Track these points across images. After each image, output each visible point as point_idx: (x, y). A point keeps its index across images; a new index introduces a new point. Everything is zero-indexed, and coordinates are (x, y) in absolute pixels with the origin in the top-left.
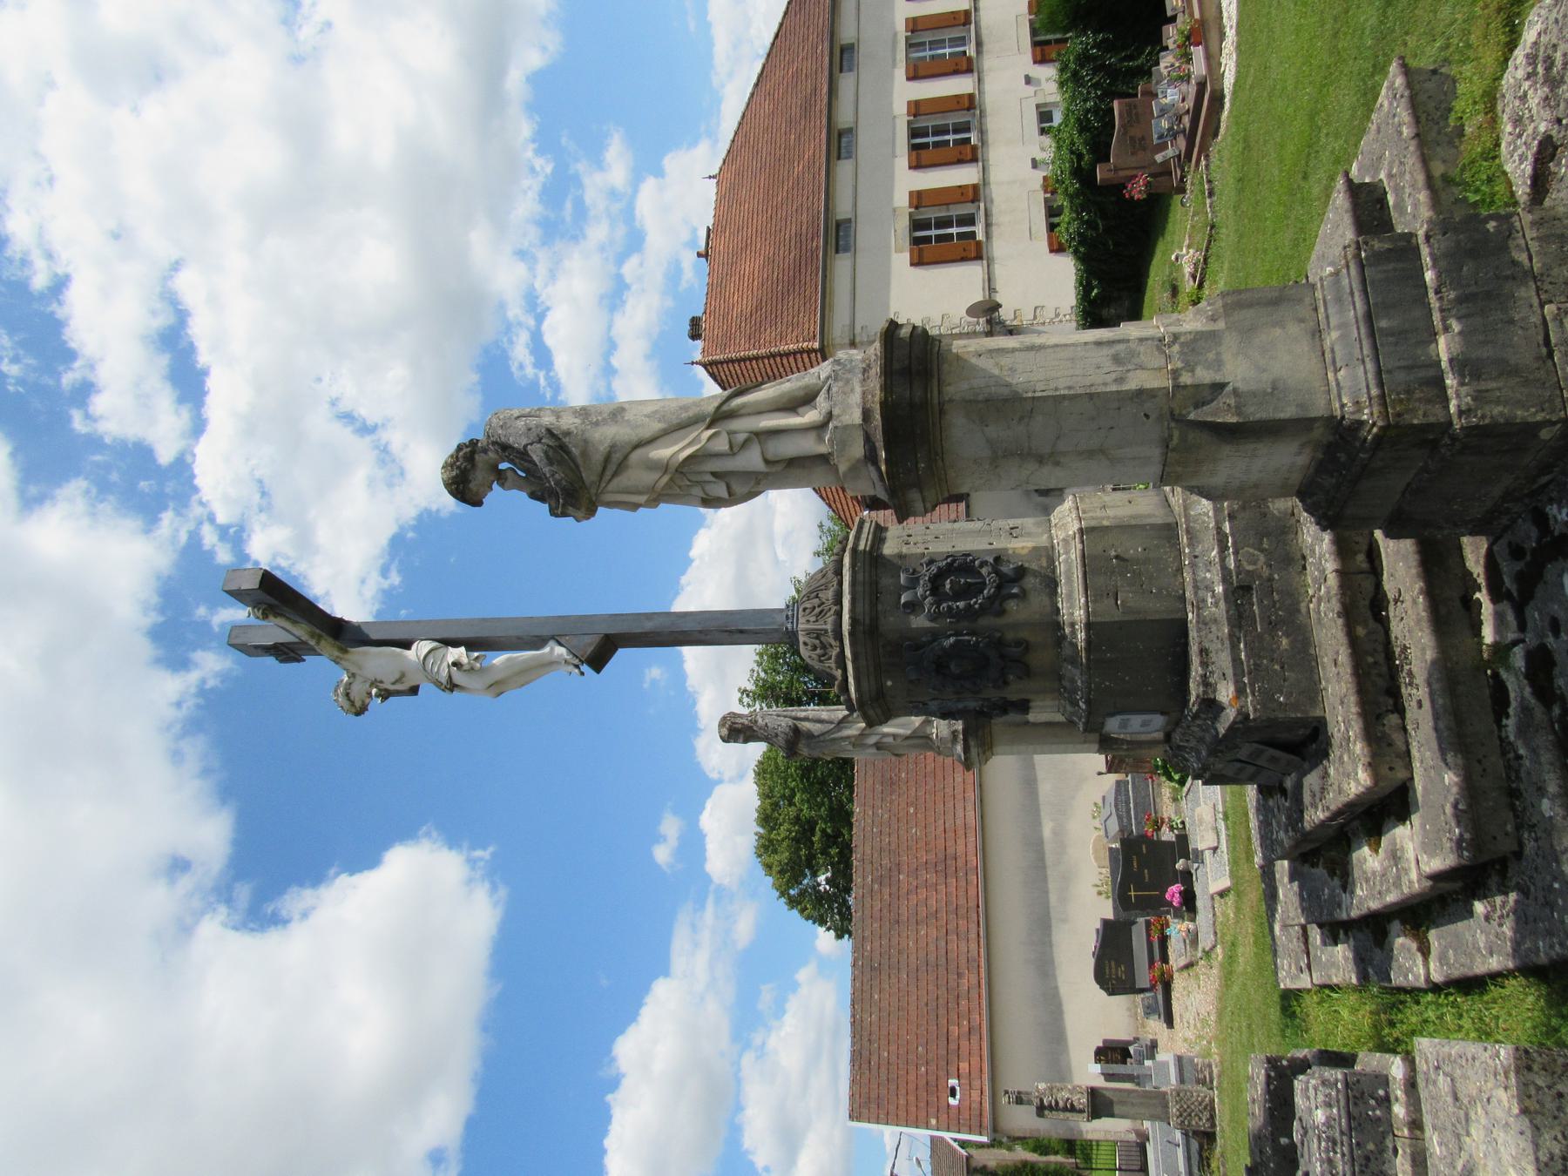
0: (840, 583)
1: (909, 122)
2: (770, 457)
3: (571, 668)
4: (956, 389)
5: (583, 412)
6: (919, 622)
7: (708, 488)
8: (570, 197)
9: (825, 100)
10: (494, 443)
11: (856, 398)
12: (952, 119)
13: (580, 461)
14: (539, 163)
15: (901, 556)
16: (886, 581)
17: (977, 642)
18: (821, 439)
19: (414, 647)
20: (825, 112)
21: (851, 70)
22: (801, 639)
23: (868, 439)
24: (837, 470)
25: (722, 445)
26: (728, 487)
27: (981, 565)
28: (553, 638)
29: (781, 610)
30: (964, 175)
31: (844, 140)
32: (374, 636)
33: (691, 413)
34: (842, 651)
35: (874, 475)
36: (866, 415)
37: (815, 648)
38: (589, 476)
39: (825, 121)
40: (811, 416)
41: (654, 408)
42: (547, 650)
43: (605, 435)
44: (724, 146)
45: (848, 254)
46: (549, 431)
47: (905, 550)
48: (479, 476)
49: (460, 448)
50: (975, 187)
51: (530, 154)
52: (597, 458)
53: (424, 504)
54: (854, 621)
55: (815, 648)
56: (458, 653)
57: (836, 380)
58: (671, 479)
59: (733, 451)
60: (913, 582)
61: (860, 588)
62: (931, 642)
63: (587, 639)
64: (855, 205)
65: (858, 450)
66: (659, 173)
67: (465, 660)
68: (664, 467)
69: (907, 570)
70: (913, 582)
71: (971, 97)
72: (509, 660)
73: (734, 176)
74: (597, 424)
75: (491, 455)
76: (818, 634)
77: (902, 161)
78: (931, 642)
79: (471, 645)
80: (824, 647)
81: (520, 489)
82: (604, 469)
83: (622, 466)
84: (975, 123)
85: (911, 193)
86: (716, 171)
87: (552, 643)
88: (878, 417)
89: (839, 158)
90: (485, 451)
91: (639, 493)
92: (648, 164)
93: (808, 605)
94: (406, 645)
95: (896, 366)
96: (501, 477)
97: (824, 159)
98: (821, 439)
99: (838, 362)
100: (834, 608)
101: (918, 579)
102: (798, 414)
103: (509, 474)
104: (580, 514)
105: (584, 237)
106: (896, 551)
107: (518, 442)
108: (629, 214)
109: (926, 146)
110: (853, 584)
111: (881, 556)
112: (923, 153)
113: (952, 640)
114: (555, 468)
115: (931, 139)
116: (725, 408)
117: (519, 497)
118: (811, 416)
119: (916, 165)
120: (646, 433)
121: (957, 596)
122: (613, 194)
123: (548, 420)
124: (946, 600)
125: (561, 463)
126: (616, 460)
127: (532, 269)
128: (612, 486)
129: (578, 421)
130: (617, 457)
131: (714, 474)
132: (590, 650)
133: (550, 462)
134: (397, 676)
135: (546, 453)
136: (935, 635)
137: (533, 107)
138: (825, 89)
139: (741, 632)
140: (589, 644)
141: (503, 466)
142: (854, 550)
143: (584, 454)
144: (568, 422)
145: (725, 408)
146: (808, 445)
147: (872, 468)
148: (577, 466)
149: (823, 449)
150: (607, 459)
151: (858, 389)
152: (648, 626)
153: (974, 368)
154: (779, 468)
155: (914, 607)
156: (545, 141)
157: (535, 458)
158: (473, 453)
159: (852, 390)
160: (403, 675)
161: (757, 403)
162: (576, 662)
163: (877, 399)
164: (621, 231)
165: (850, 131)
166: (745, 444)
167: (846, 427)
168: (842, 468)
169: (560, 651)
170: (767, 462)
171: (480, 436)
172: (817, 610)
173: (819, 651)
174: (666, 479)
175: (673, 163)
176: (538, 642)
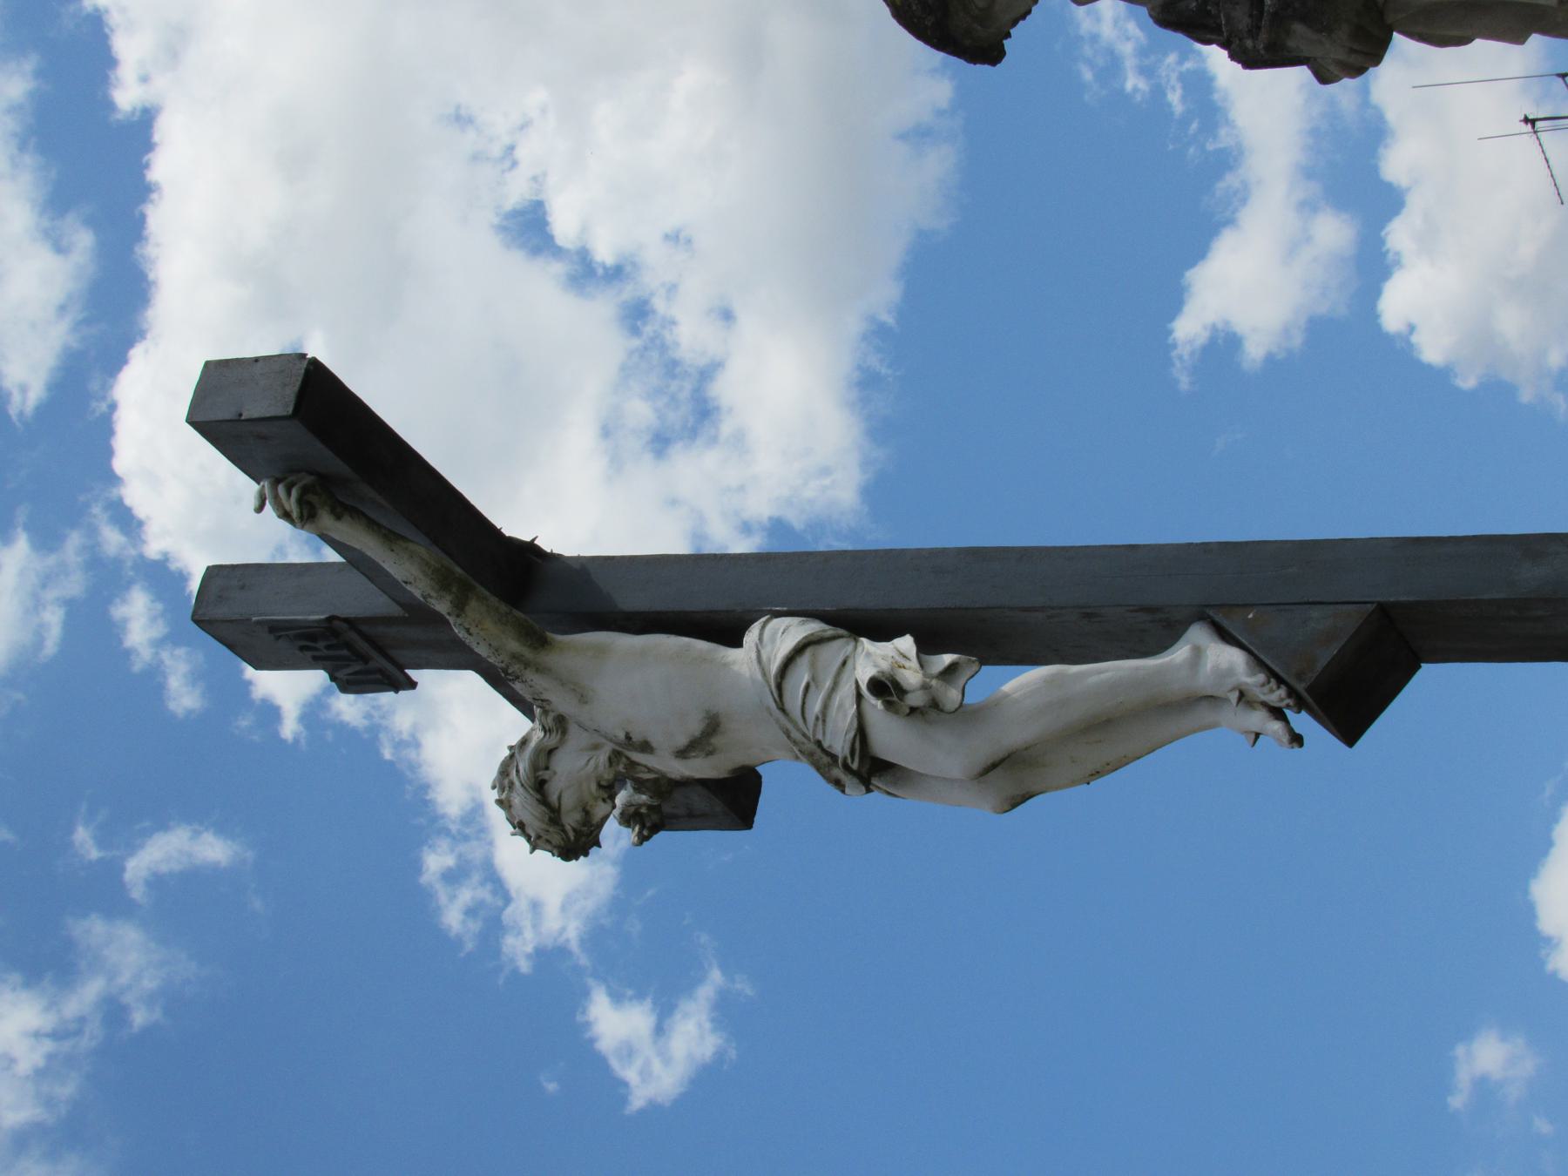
19: (751, 637)
42: (1179, 654)
67: (911, 676)
72: (1050, 681)
87: (1198, 634)
134: (695, 727)
140: (1324, 634)
160: (713, 725)
162: (1277, 696)
176: (1155, 632)
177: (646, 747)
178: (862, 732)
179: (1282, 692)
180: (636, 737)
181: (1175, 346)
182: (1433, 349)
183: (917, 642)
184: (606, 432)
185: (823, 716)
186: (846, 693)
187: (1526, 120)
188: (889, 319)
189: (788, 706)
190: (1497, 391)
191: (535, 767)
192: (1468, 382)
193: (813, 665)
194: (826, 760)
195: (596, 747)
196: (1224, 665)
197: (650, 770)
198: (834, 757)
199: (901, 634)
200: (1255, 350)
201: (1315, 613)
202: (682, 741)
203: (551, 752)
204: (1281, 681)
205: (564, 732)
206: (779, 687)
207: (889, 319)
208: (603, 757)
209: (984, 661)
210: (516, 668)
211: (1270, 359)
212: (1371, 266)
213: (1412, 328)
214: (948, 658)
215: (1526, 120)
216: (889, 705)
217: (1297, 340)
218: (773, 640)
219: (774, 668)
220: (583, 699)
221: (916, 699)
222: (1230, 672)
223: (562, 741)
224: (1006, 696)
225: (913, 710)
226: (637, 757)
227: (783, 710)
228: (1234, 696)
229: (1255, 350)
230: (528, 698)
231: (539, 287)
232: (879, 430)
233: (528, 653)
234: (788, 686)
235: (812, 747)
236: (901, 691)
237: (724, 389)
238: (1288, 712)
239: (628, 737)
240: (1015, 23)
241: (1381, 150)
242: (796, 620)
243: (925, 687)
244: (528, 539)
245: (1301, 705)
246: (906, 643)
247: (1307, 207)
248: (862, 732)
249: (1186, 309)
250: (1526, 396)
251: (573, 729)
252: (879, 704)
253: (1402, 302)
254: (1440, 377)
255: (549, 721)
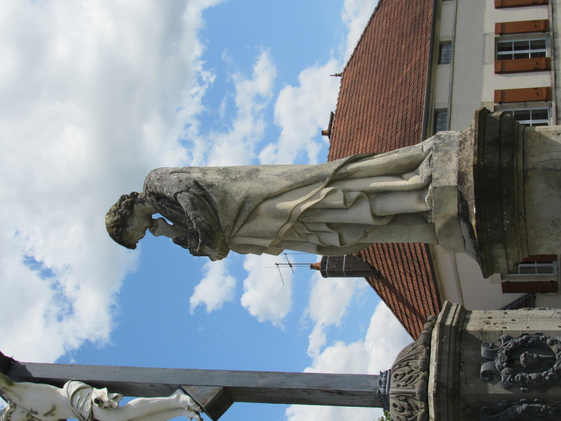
0: (429, 353)
1: (496, 39)
2: (378, 212)
3: (192, 414)
4: (538, 159)
5: (225, 171)
6: (496, 389)
7: (322, 236)
8: (225, 98)
9: (430, 20)
10: (152, 193)
11: (453, 166)
12: (530, 39)
13: (219, 208)
14: (206, 75)
15: (482, 332)
16: (468, 353)
17: (546, 410)
18: (421, 199)
19: (66, 386)
20: (430, 28)
21: (448, 63)
22: (392, 401)
23: (462, 199)
24: (434, 229)
25: (337, 200)
26: (340, 237)
27: (552, 343)
28: (180, 387)
29: (375, 377)
30: (539, 80)
31: (444, 50)
32: (35, 375)
33: (313, 174)
34: (427, 412)
35: (465, 232)
36: (461, 177)
37: (403, 410)
38: (225, 221)
39: (429, 35)
40: (414, 180)
41: (285, 170)
42: (174, 396)
43: (240, 189)
44: (347, 58)
45: (448, 65)
46: (196, 183)
47: (486, 328)
48: (136, 222)
49: (123, 198)
50: (548, 90)
51: (199, 68)
52: (233, 206)
53: (84, 336)
54: (439, 384)
55: (403, 410)
56: (102, 393)
57: (436, 151)
58: (293, 227)
59: (347, 206)
60: (492, 355)
61: (445, 357)
62: (506, 407)
63: (209, 390)
64: (451, 98)
65: (452, 208)
66: (296, 84)
67: (106, 398)
68: (287, 216)
69: (487, 345)
70: (492, 355)
71: (546, 22)
72: (141, 402)
73: (354, 77)
74: (235, 180)
75: (147, 205)
76: (406, 397)
77: (490, 68)
78: (506, 407)
79: (112, 388)
80: (411, 409)
81: (168, 235)
82: (238, 216)
83: (253, 214)
84: (548, 42)
85: (496, 92)
86: (342, 71)
87: (179, 391)
88: (471, 178)
89: (439, 63)
90: (143, 201)
91: (265, 237)
92: (287, 76)
93: (399, 372)
94: (60, 384)
95: (488, 138)
96: (153, 226)
97: (427, 63)
98: (421, 199)
99: (439, 137)
100: (422, 374)
101: (496, 352)
102: (403, 179)
103: (160, 223)
104: (215, 254)
105: (232, 128)
106: (478, 328)
107: (169, 191)
108: (269, 114)
109: (510, 56)
110: (440, 352)
111: (465, 332)
112: (507, 62)
113: (524, 406)
114: (198, 212)
115: (513, 52)
116: (342, 171)
117: (166, 242)
118: (414, 180)
119: (500, 71)
120: (276, 188)
121: (529, 369)
122: (258, 98)
123: (196, 175)
124: (520, 372)
125: (203, 208)
126: (249, 209)
127: (190, 154)
128: (241, 232)
129: (220, 177)
130: (250, 206)
131: (329, 225)
132: (209, 399)
133: (194, 207)
134: (49, 409)
135: (192, 200)
136: (510, 402)
137: (203, 35)
138: (430, 13)
139: (340, 393)
140: (209, 394)
141: (156, 216)
142: (442, 324)
143: (223, 202)
144: (211, 178)
145: (342, 171)
146: (411, 204)
147: (463, 225)
148: (216, 212)
149: (423, 207)
150: (242, 207)
151: (455, 159)
152: (261, 382)
153: (554, 144)
154: (385, 222)
155: (492, 375)
156: (210, 60)
157: (183, 204)
158: (133, 202)
159: (450, 159)
160: (54, 408)
161: (368, 167)
162: (197, 409)
163: (471, 163)
164: (261, 126)
165: (449, 43)
166: (357, 201)
167: (443, 188)
168: (439, 225)
169: (185, 398)
170: (374, 216)
171: (140, 190)
172: (407, 376)
173: (406, 413)
174: (288, 226)
175: (307, 77)
176: (168, 390)
177: (36, 413)
178: (92, 412)
179: (199, 407)
180: (34, 410)
181: (190, 304)
182: (253, 312)
183: (108, 390)
184: (45, 316)
185: (82, 408)
186: (89, 401)
187: (276, 264)
188: (118, 292)
189: (74, 404)
190: (268, 323)
191: (7, 417)
192: (261, 320)
193: (81, 395)
194: (82, 419)
195: (23, 412)
196: (185, 400)
197: (37, 419)
198: (84, 418)
199: (104, 387)
200: (210, 308)
201: (208, 388)
202: (46, 412)
203: (11, 413)
204: (198, 405)
205: (15, 408)
206: (72, 399)
207: (118, 292)
208: (25, 415)
209: (124, 395)
210: (4, 390)
211: (213, 311)
212: (239, 290)
213: (248, 306)
214: (115, 394)
215: (276, 264)
216: (99, 405)
217: (221, 307)
218: (71, 387)
219: (71, 394)
220: (21, 399)
221: (106, 405)
222: (186, 402)
223: (14, 410)
224: (129, 405)
225: (105, 407)
226: (34, 415)
227: (72, 405)
228: (187, 408)
229: (210, 308)
230: (7, 398)
231: (33, 276)
232: (116, 319)
233: (7, 387)
234: (74, 399)
235: (79, 415)
236: (103, 402)
237: (76, 305)
238: (200, 413)
239: (32, 410)
240: (139, 239)
241: (244, 263)
242: (78, 382)
243: (109, 401)
244: (10, 357)
245: (203, 411)
246: (105, 390)
247: (225, 275)
248: (92, 412)
249: (194, 296)
250: (274, 324)
251: (18, 407)
252: (97, 405)
253: (245, 300)
254: (255, 318)
255: (12, 405)
